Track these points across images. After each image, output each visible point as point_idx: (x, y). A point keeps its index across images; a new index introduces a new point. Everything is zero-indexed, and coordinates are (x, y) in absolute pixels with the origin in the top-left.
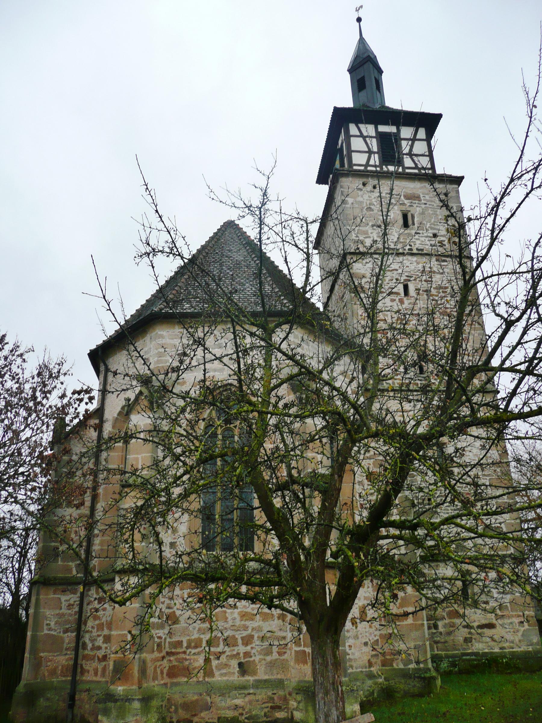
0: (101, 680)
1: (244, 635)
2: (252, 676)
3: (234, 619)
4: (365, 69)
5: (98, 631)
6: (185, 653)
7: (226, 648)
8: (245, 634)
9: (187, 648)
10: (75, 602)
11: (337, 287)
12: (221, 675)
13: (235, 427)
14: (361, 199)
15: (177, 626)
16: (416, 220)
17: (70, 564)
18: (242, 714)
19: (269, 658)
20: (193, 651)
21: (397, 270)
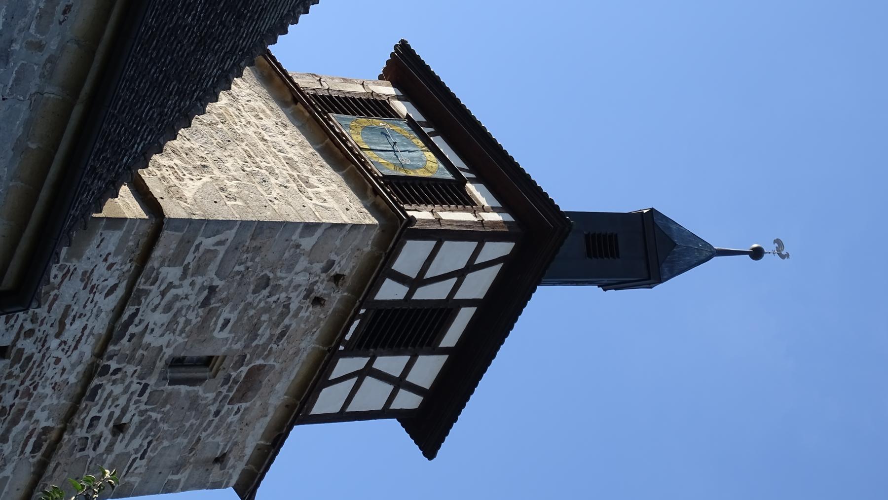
11: (58, 469)
14: (299, 267)
16: (183, 389)
21: (58, 336)
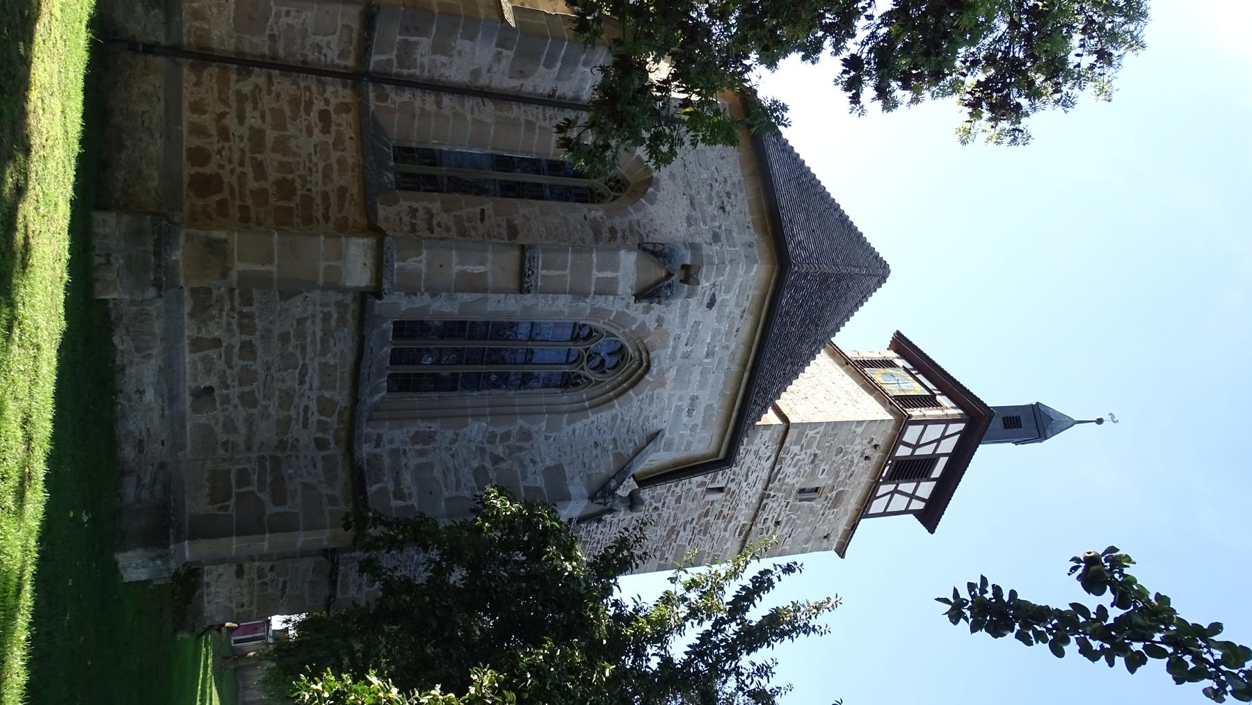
0: (185, 124)
1: (257, 394)
3: (283, 381)
4: (1031, 424)
5: (273, 111)
6: (232, 309)
7: (236, 369)
9: (241, 313)
12: (194, 363)
13: (582, 369)
16: (806, 503)
17: (395, 53)
18: (130, 400)
19: (219, 429)
20: (234, 322)
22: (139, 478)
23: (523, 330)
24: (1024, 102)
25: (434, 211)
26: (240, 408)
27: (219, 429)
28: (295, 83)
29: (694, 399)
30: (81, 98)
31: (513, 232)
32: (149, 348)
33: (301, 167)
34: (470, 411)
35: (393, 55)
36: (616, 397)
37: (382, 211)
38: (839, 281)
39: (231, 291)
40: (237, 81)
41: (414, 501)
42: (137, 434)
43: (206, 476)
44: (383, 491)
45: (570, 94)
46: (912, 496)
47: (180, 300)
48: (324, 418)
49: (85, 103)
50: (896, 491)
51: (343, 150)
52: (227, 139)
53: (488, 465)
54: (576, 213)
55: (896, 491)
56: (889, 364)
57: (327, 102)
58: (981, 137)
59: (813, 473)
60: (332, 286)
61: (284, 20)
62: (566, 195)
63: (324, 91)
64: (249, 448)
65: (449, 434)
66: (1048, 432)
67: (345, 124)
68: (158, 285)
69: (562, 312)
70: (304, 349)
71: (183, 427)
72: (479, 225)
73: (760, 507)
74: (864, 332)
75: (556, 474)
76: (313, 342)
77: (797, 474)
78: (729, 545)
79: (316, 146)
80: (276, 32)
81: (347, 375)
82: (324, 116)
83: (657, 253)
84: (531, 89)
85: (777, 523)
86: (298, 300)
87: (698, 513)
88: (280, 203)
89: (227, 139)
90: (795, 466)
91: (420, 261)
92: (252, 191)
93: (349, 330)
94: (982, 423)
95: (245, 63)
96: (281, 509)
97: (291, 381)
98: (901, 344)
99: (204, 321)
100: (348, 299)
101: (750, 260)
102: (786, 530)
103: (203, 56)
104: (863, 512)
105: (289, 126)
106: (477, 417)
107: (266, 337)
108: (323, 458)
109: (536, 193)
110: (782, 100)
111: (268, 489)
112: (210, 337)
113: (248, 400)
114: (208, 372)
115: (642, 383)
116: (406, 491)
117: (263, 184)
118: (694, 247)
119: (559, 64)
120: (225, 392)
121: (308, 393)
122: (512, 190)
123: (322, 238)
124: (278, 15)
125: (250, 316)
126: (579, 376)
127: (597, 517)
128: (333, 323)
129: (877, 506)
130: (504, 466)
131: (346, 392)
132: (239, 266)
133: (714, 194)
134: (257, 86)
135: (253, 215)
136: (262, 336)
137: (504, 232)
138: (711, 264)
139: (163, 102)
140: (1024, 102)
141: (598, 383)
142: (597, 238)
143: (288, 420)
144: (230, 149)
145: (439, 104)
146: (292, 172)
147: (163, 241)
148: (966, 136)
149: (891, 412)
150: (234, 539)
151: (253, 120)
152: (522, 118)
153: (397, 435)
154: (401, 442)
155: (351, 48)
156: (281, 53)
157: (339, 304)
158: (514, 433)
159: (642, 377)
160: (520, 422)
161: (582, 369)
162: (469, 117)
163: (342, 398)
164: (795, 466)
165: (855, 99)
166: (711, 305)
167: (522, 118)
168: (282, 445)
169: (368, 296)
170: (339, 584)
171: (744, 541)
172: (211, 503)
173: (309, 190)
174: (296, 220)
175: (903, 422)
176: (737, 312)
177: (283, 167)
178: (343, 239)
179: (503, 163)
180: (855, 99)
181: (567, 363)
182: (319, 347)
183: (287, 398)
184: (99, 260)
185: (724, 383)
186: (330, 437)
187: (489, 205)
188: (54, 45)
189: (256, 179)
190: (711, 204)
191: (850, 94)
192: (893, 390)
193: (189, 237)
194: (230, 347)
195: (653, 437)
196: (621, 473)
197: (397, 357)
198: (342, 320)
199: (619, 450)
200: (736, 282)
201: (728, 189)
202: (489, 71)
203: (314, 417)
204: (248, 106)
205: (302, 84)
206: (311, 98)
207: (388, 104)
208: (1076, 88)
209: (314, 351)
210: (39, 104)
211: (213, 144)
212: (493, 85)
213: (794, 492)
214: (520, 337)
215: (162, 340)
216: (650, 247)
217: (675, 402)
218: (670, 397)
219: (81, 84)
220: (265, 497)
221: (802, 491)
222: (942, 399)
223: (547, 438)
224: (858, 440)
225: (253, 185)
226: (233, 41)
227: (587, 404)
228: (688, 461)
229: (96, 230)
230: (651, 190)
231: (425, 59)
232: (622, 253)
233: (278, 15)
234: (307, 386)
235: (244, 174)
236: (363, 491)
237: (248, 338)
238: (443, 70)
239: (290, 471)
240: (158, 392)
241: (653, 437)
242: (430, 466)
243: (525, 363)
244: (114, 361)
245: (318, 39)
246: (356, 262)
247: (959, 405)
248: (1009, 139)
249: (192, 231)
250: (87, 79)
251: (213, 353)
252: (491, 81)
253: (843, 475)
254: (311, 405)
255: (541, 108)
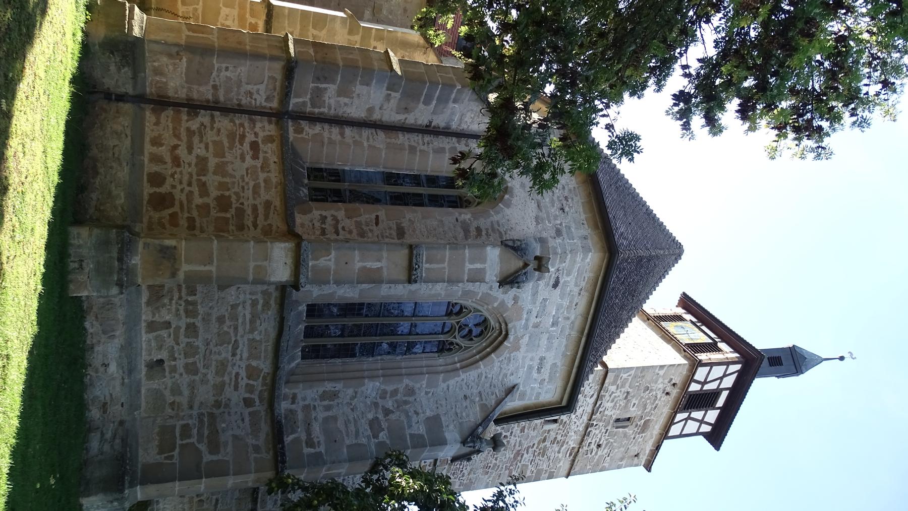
1: (198, 365)
2: (146, 375)
3: (219, 353)
4: (790, 362)
5: (214, 142)
6: (180, 298)
7: (182, 345)
8: (200, 365)
9: (186, 301)
10: (255, 100)
13: (455, 337)
15: (216, 289)
16: (621, 430)
17: (309, 96)
18: (97, 371)
20: (182, 308)
22: (102, 434)
23: (408, 310)
24: (825, 124)
25: (339, 218)
26: (185, 376)
27: (167, 393)
28: (232, 121)
29: (542, 359)
30: (62, 138)
31: (401, 233)
32: (113, 331)
33: (236, 185)
34: (366, 373)
35: (307, 99)
36: (482, 359)
37: (299, 219)
38: (650, 260)
39: (179, 286)
40: (187, 121)
41: (322, 449)
42: (102, 398)
43: (157, 430)
44: (297, 441)
45: (442, 125)
46: (702, 422)
47: (139, 293)
48: (251, 382)
49: (66, 143)
50: (689, 418)
51: (269, 172)
52: (179, 166)
53: (381, 416)
54: (448, 217)
55: (689, 418)
56: (679, 318)
57: (256, 134)
58: (787, 154)
59: (626, 406)
60: (258, 281)
61: (224, 74)
62: (436, 201)
63: (254, 127)
64: (191, 407)
65: (350, 391)
66: (803, 368)
67: (270, 151)
68: (120, 284)
69: (440, 295)
70: (236, 328)
71: (139, 392)
72: (374, 228)
73: (586, 433)
74: (662, 299)
75: (434, 422)
76: (244, 323)
77: (614, 408)
78: (561, 464)
79: (247, 169)
80: (218, 84)
81: (270, 348)
82: (254, 146)
83: (515, 247)
84: (412, 122)
85: (599, 446)
86: (232, 290)
87: (538, 439)
88: (219, 215)
89: (179, 166)
90: (613, 401)
91: (330, 260)
92: (197, 206)
93: (272, 312)
94: (754, 363)
95: (193, 107)
96: (215, 458)
97: (225, 353)
98: (687, 302)
99: (157, 308)
100: (272, 289)
101: (586, 249)
102: (606, 451)
103: (161, 103)
104: (665, 435)
105: (227, 154)
106: (372, 378)
107: (206, 320)
108: (250, 414)
109: (417, 201)
110: (637, 131)
111: (206, 441)
112: (163, 320)
113: (191, 369)
114: (160, 348)
115: (502, 347)
116: (316, 440)
117: (206, 200)
118: (542, 241)
119: (434, 102)
120: (173, 363)
121: (238, 363)
122: (399, 200)
123: (252, 243)
124: (219, 70)
125: (194, 303)
126: (452, 343)
127: (467, 457)
128: (260, 307)
129: (675, 430)
130: (393, 417)
131: (269, 362)
132: (185, 268)
133: (555, 198)
134: (202, 124)
135: (198, 224)
136: (203, 319)
137: (394, 233)
138: (556, 253)
139: (129, 138)
140: (825, 124)
141: (466, 348)
142: (466, 237)
143: (223, 384)
144: (181, 173)
145: (342, 134)
146: (228, 190)
147: (125, 249)
148: (773, 154)
149: (685, 357)
150: (177, 483)
151: (199, 150)
152: (407, 144)
153: (308, 394)
154: (312, 399)
155: (276, 94)
156: (222, 99)
157: (264, 293)
158: (401, 390)
159: (501, 343)
160: (406, 381)
161: (455, 337)
162: (365, 144)
163: (265, 365)
164: (613, 401)
165: (686, 126)
166: (555, 285)
167: (407, 144)
168: (217, 404)
169: (285, 291)
170: (259, 500)
171: (573, 461)
172: (159, 453)
173: (242, 204)
174: (231, 228)
175: (696, 364)
176: (576, 290)
177: (222, 186)
178: (269, 244)
179: (391, 178)
180: (686, 126)
181: (443, 333)
182: (248, 326)
183: (222, 367)
184: (73, 265)
185: (566, 346)
186: (255, 397)
187: (382, 211)
188: (38, 99)
189: (201, 196)
190: (553, 206)
191: (682, 123)
192: (685, 339)
193: (146, 245)
194: (178, 328)
195: (511, 390)
196: (485, 422)
197: (309, 332)
198: (266, 304)
199: (484, 402)
200: (577, 267)
201: (566, 194)
202: (380, 108)
203: (243, 382)
204: (196, 140)
205: (237, 122)
206: (244, 132)
207: (304, 135)
208: (866, 111)
209: (244, 330)
210: (20, 148)
211: (168, 169)
212: (384, 119)
213: (612, 422)
214: (406, 314)
215: (123, 324)
216: (510, 243)
217: (528, 362)
218: (524, 358)
219: (62, 127)
220: (203, 447)
221: (618, 420)
222: (722, 345)
223: (427, 393)
224: (660, 380)
225: (198, 200)
226: (185, 90)
227: (458, 365)
228: (536, 406)
229: (72, 242)
230: (507, 196)
231: (333, 101)
232: (489, 248)
233: (219, 70)
234: (238, 357)
235: (191, 192)
236: (281, 441)
237: (192, 321)
238: (345, 109)
239: (223, 425)
240: (120, 366)
241: (511, 390)
242: (335, 418)
243: (410, 334)
244: (85, 342)
245: (249, 87)
246: (279, 263)
247: (736, 350)
248: (813, 155)
249: (149, 240)
250: (68, 124)
251: (164, 333)
252: (382, 116)
253: (649, 407)
254: (241, 371)
255: (420, 135)
